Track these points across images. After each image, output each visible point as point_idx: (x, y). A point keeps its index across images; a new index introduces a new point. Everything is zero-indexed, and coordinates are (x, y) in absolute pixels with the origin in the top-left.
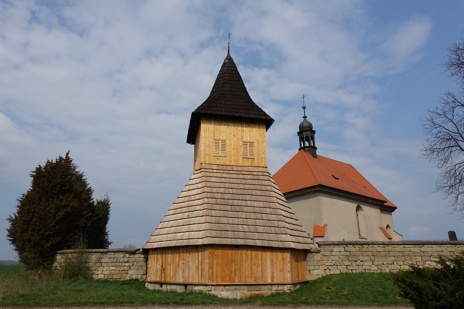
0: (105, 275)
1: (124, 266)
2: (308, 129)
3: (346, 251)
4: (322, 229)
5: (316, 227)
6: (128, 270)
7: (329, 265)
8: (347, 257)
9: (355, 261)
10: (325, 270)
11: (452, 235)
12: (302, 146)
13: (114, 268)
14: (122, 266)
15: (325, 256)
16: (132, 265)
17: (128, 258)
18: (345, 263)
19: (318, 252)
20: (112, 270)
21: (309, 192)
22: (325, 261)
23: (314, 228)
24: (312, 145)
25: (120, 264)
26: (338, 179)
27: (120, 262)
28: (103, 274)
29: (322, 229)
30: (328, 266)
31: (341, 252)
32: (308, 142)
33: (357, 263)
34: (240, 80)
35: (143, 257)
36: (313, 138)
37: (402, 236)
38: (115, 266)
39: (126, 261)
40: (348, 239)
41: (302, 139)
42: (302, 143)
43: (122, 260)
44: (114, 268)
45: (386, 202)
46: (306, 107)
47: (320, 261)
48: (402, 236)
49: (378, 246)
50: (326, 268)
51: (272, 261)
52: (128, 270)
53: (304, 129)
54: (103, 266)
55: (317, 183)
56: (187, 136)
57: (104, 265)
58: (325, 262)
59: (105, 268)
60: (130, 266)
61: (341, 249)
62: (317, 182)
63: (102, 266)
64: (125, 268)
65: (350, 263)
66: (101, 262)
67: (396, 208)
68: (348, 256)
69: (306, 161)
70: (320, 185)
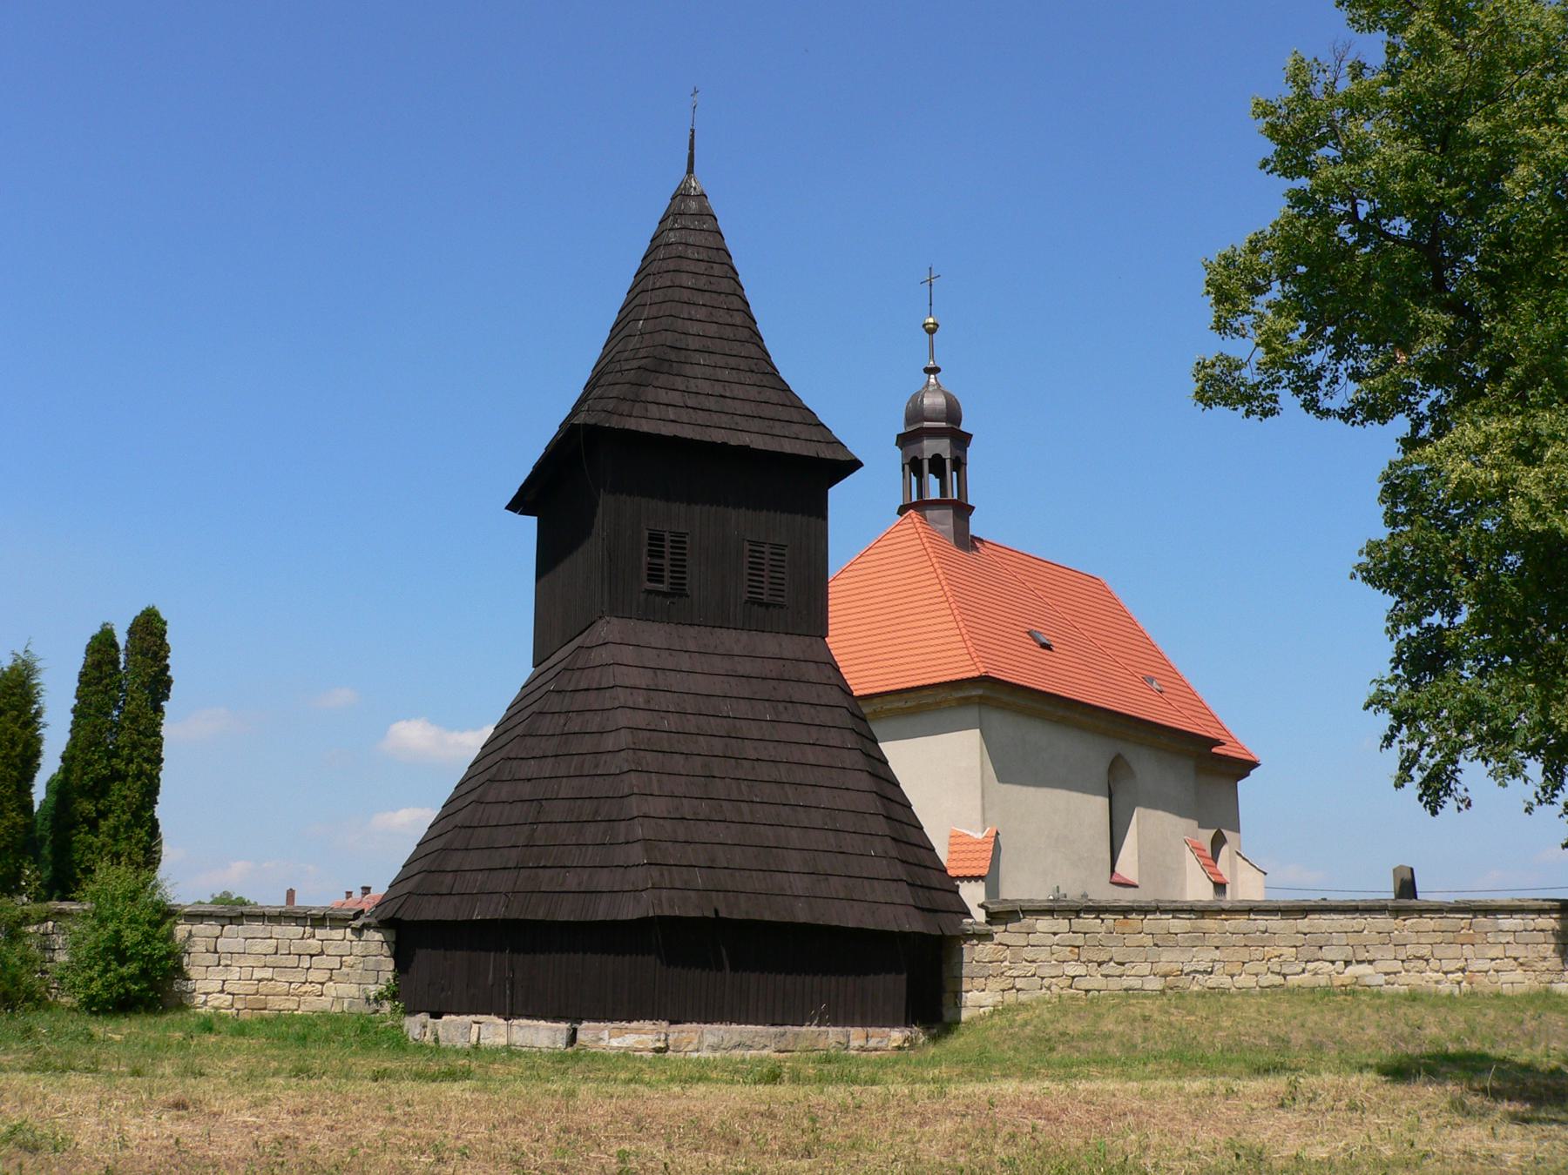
0: (233, 995)
1: (308, 969)
2: (943, 424)
3: (1073, 932)
4: (978, 847)
5: (959, 840)
6: (322, 984)
7: (1018, 977)
8: (1076, 950)
9: (1100, 964)
10: (1003, 991)
11: (1407, 887)
12: (915, 499)
13: (268, 973)
14: (298, 967)
15: (1008, 946)
16: (338, 966)
17: (322, 941)
18: (1069, 968)
19: (988, 937)
20: (260, 981)
21: (938, 704)
22: (1006, 963)
23: (950, 844)
24: (956, 497)
25: (293, 960)
26: (1051, 650)
27: (289, 954)
28: (229, 994)
29: (978, 847)
30: (1015, 977)
31: (1057, 937)
32: (937, 477)
33: (1105, 969)
34: (735, 290)
35: (383, 939)
36: (959, 464)
37: (1265, 874)
38: (274, 968)
39: (312, 952)
40: (1072, 893)
41: (914, 466)
42: (914, 479)
43: (297, 946)
44: (268, 973)
45: (1218, 743)
46: (938, 326)
47: (990, 962)
48: (1265, 874)
49: (1173, 918)
50: (1007, 984)
51: (495, 960)
52: (322, 984)
53: (927, 424)
54: (226, 966)
55: (974, 667)
56: (523, 481)
57: (229, 963)
58: (1006, 966)
59: (235, 973)
60: (332, 970)
61: (1062, 924)
62: (975, 664)
63: (222, 963)
64: (314, 975)
65: (1081, 970)
66: (216, 952)
67: (1254, 765)
68: (1078, 947)
69: (931, 569)
70: (984, 680)
